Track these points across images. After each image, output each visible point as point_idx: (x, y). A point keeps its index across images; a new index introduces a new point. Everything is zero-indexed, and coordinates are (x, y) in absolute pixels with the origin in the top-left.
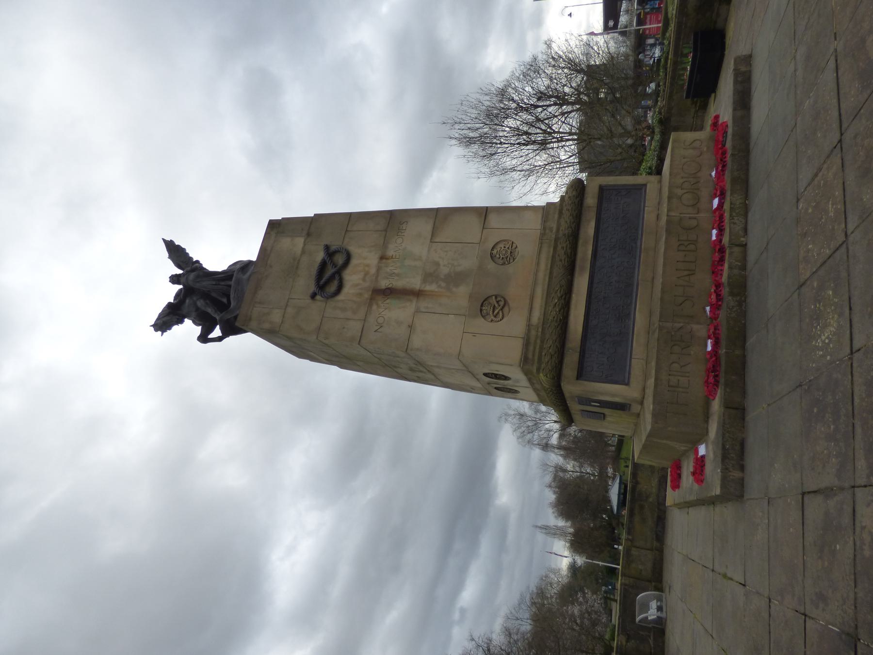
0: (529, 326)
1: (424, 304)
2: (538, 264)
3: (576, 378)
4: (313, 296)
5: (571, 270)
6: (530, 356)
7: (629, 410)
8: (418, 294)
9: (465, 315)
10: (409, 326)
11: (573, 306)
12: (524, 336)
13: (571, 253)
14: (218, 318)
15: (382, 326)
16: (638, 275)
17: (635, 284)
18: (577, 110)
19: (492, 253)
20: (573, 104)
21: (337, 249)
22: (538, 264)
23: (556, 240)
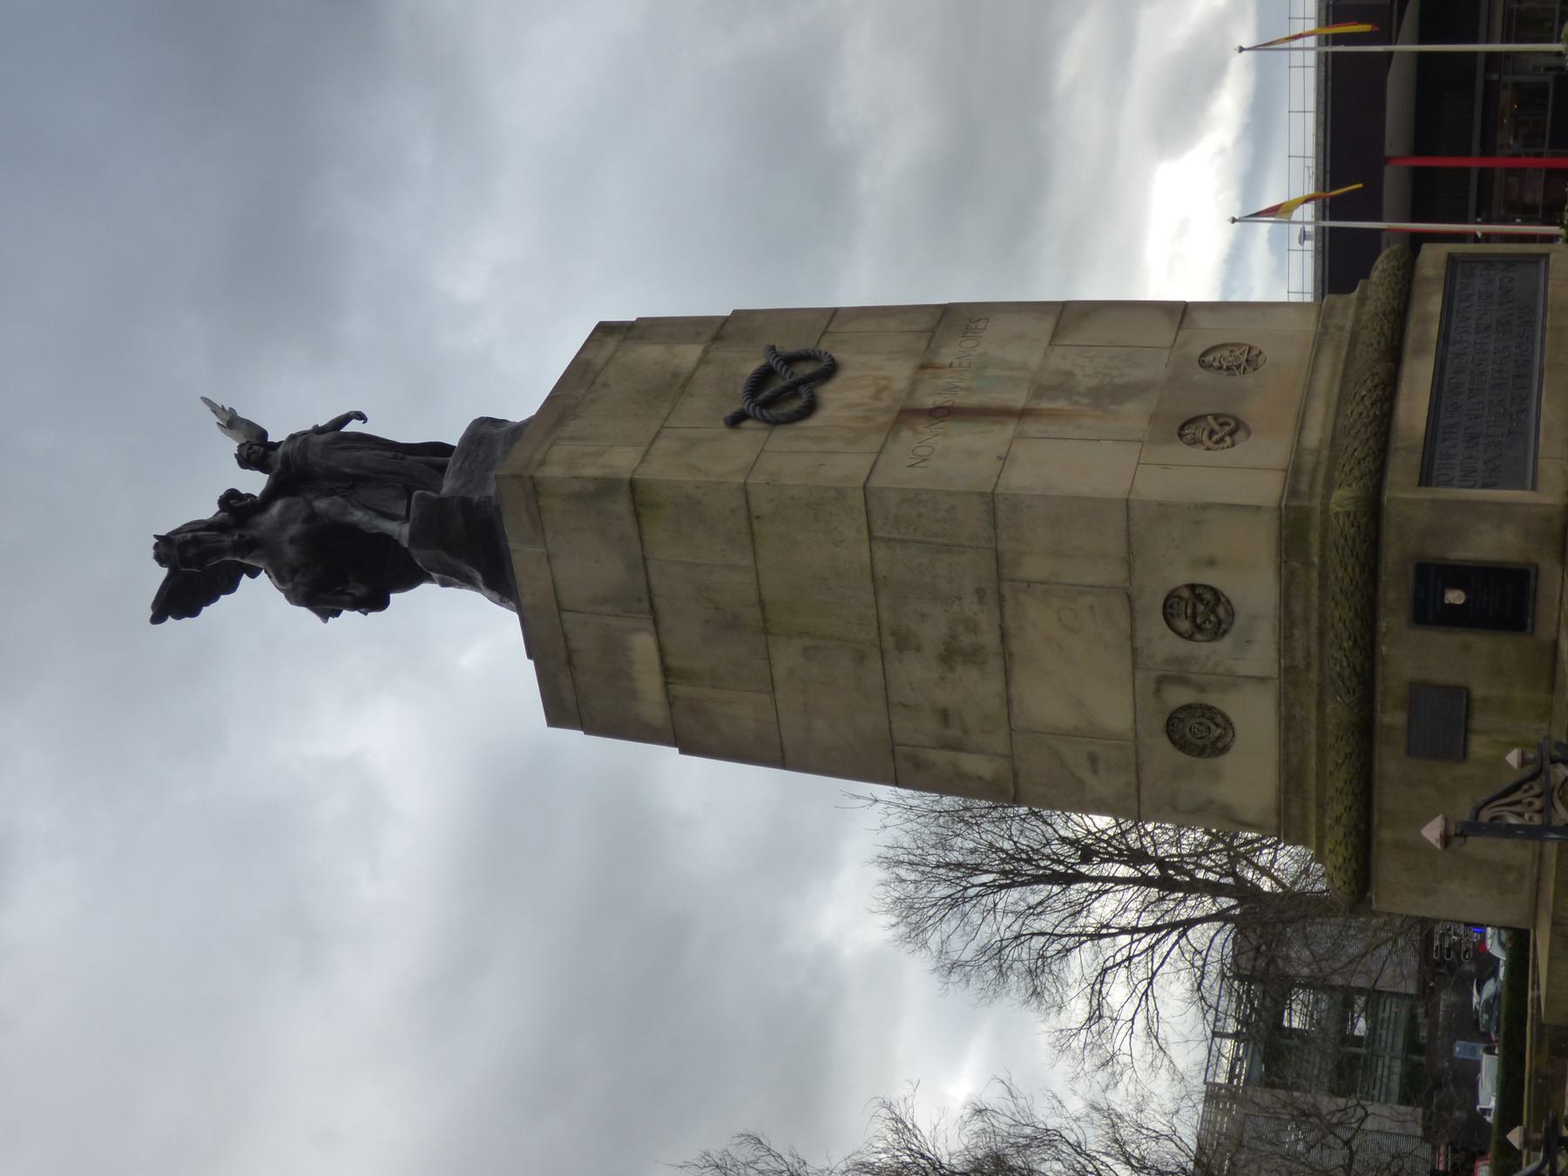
0: (1298, 450)
1: (1032, 427)
2: (1313, 370)
3: (1416, 479)
4: (736, 421)
5: (1394, 354)
6: (1303, 486)
7: (1532, 633)
8: (1022, 414)
9: (1139, 441)
10: (999, 458)
11: (1404, 387)
12: (1285, 468)
13: (1393, 335)
14: (401, 531)
15: (926, 460)
16: (1545, 315)
17: (1536, 375)
18: (1221, 916)
19: (1203, 361)
20: (1215, 890)
21: (812, 354)
22: (1313, 370)
23: (1354, 336)
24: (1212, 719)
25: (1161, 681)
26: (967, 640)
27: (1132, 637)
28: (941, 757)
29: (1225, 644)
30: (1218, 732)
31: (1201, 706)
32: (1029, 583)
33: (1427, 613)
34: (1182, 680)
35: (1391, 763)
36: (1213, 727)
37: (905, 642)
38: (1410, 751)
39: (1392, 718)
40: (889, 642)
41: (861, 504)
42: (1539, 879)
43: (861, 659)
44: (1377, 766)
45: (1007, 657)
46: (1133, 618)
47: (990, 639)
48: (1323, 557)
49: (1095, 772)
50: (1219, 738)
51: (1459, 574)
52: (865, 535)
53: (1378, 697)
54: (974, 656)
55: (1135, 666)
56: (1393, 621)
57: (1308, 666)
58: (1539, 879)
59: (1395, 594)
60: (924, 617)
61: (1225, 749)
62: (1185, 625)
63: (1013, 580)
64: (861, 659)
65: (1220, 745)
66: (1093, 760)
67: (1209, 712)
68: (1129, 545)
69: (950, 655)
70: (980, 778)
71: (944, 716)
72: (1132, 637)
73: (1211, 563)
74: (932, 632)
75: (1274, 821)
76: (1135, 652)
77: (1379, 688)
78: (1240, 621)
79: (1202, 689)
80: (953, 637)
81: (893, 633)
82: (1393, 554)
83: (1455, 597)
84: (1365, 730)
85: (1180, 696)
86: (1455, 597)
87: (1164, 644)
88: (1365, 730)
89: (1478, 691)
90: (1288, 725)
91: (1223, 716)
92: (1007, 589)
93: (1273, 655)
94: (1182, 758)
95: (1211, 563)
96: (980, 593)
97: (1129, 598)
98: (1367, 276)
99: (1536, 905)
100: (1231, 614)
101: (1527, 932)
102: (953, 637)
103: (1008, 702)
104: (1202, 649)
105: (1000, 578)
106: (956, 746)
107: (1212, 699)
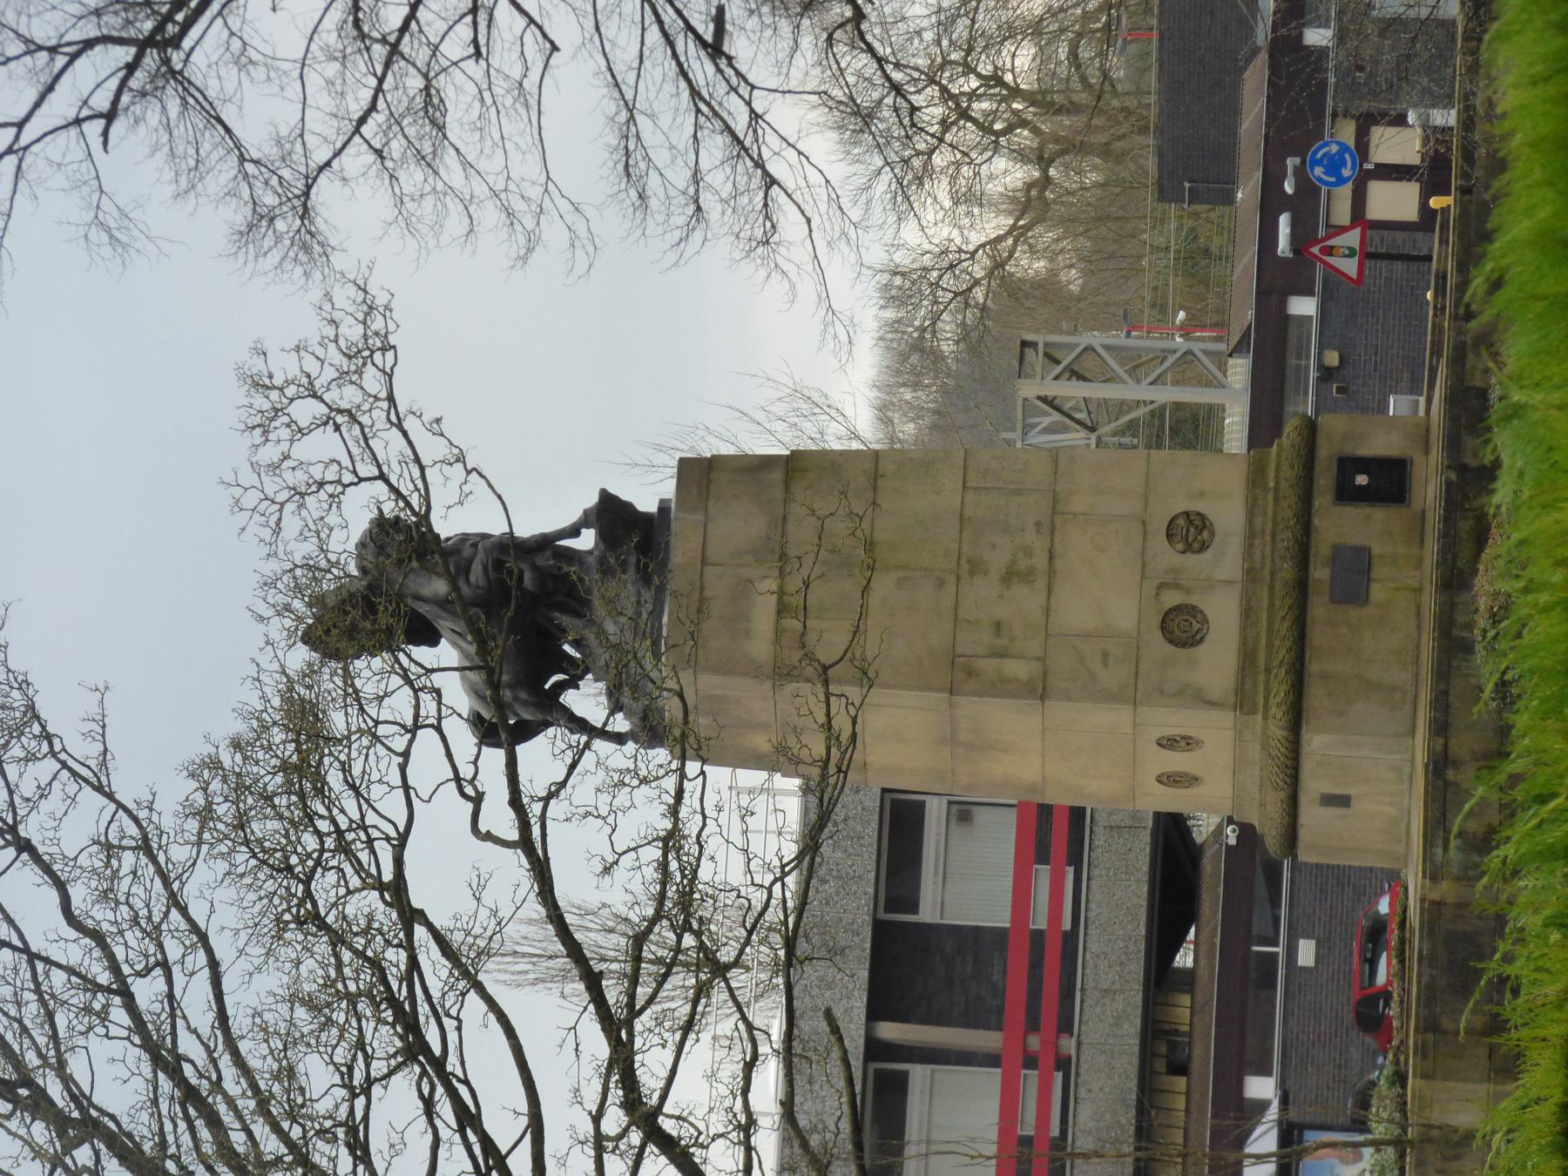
7: (1409, 506)
24: (1194, 617)
25: (1161, 586)
26: (1023, 563)
27: (1143, 554)
28: (987, 665)
29: (1208, 554)
30: (1196, 626)
31: (1186, 606)
32: (1074, 515)
33: (1346, 494)
34: (1176, 586)
35: (1319, 608)
36: (1194, 623)
37: (976, 567)
38: (1333, 600)
39: (1320, 573)
40: (965, 566)
41: (961, 463)
42: (1416, 696)
43: (941, 584)
44: (1309, 613)
45: (1051, 573)
46: (1145, 539)
47: (1040, 562)
48: (1277, 483)
49: (1106, 666)
50: (1199, 630)
51: (1364, 464)
52: (960, 485)
53: (1312, 559)
54: (1027, 577)
55: (1143, 577)
56: (1323, 499)
57: (1262, 569)
58: (1416, 696)
59: (1325, 480)
60: (994, 546)
61: (1201, 640)
62: (1180, 546)
63: (1063, 513)
64: (941, 584)
65: (1198, 637)
66: (1105, 655)
67: (1192, 610)
68: (1147, 483)
69: (1011, 576)
70: (1017, 680)
71: (998, 627)
72: (1143, 554)
73: (1202, 495)
74: (998, 560)
75: (1232, 699)
76: (1144, 565)
77: (1313, 551)
78: (1217, 538)
79: (1188, 591)
80: (1014, 562)
81: (969, 562)
82: (1325, 452)
83: (1362, 480)
84: (1302, 587)
85: (1172, 599)
86: (1362, 480)
87: (1166, 556)
88: (1302, 587)
89: (1376, 549)
90: (1247, 612)
91: (1202, 612)
92: (1058, 520)
93: (1239, 562)
94: (1171, 649)
95: (1202, 495)
96: (1038, 524)
97: (1144, 522)
98: (1280, 436)
99: (1419, 627)
100: (1213, 533)
101: (1398, 873)
102: (1014, 562)
103: (1047, 612)
104: (1191, 559)
105: (1054, 513)
106: (1001, 654)
107: (1194, 600)
